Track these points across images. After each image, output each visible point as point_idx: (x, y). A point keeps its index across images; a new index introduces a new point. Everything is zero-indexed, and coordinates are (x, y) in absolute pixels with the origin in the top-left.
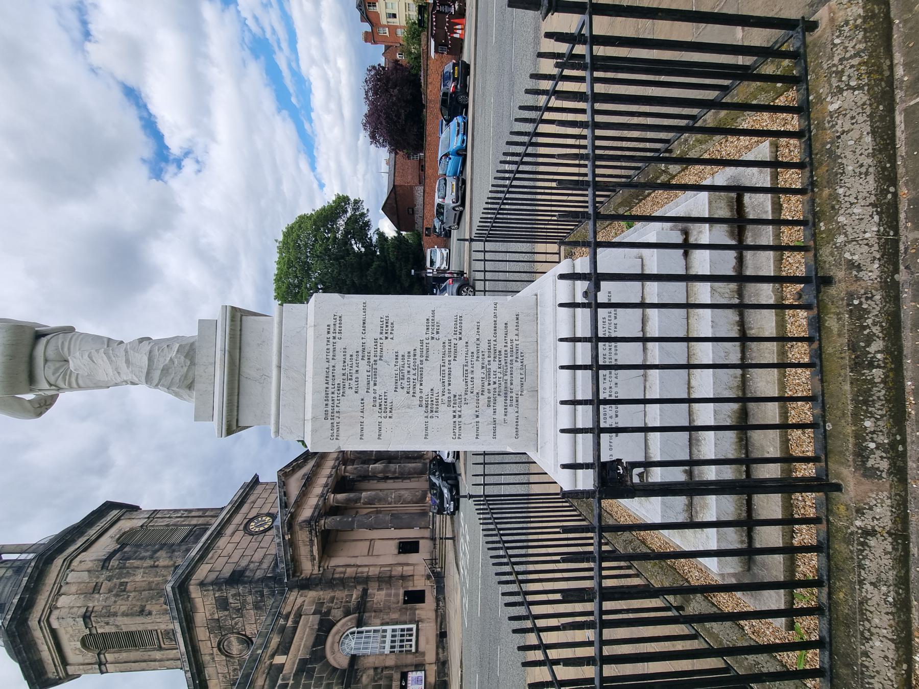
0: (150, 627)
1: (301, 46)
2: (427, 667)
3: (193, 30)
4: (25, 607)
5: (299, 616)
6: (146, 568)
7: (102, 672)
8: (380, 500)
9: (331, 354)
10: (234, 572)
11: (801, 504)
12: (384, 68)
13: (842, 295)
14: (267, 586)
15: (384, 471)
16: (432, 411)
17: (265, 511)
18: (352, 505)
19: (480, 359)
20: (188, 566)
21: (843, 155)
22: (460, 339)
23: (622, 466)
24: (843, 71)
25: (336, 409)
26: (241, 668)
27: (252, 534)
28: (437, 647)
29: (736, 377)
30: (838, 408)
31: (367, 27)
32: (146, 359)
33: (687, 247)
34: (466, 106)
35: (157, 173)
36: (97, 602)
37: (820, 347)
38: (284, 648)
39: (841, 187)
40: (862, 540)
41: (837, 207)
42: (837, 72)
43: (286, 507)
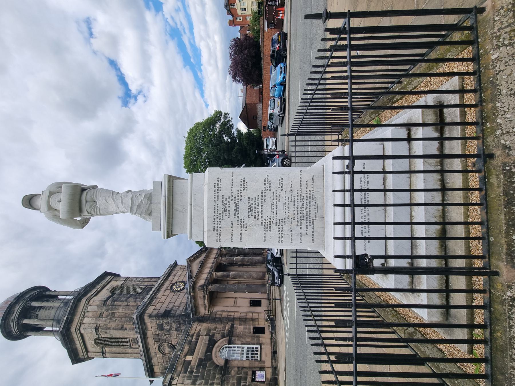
0: (126, 337)
1: (195, 31)
2: (266, 369)
3: (141, 28)
4: (69, 322)
5: (198, 336)
6: (124, 306)
7: (104, 357)
8: (240, 277)
9: (216, 198)
10: (166, 311)
11: (478, 283)
12: (239, 39)
13: (500, 164)
14: (182, 319)
15: (241, 261)
16: (267, 228)
17: (181, 280)
18: (225, 279)
19: (293, 200)
20: (143, 307)
21: (500, 84)
22: (282, 190)
23: (368, 257)
24: (500, 36)
25: (219, 226)
26: (170, 361)
27: (174, 292)
28: (272, 359)
29: (439, 211)
30: (497, 229)
31: (230, 17)
32: (130, 200)
33: (409, 139)
34: (286, 57)
35: (125, 104)
36: (101, 322)
37: (486, 194)
38: (191, 352)
39: (499, 102)
40: (511, 303)
41: (496, 114)
42: (496, 37)
43: (191, 278)
